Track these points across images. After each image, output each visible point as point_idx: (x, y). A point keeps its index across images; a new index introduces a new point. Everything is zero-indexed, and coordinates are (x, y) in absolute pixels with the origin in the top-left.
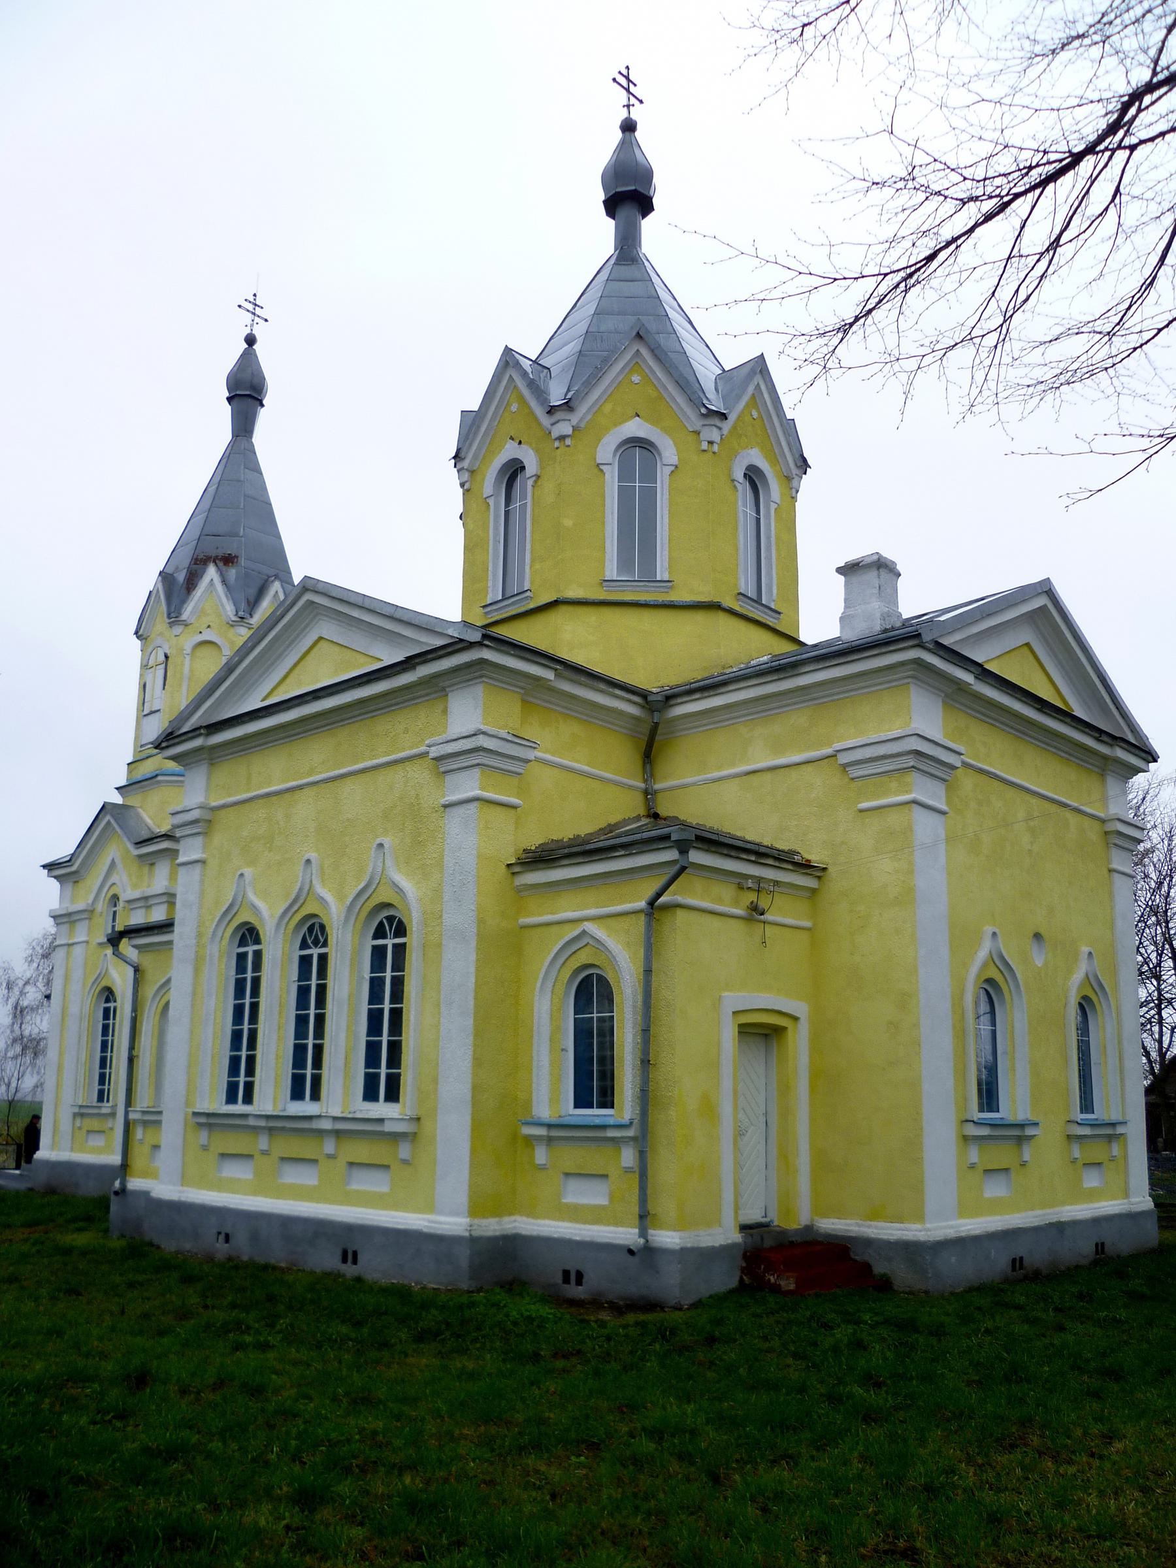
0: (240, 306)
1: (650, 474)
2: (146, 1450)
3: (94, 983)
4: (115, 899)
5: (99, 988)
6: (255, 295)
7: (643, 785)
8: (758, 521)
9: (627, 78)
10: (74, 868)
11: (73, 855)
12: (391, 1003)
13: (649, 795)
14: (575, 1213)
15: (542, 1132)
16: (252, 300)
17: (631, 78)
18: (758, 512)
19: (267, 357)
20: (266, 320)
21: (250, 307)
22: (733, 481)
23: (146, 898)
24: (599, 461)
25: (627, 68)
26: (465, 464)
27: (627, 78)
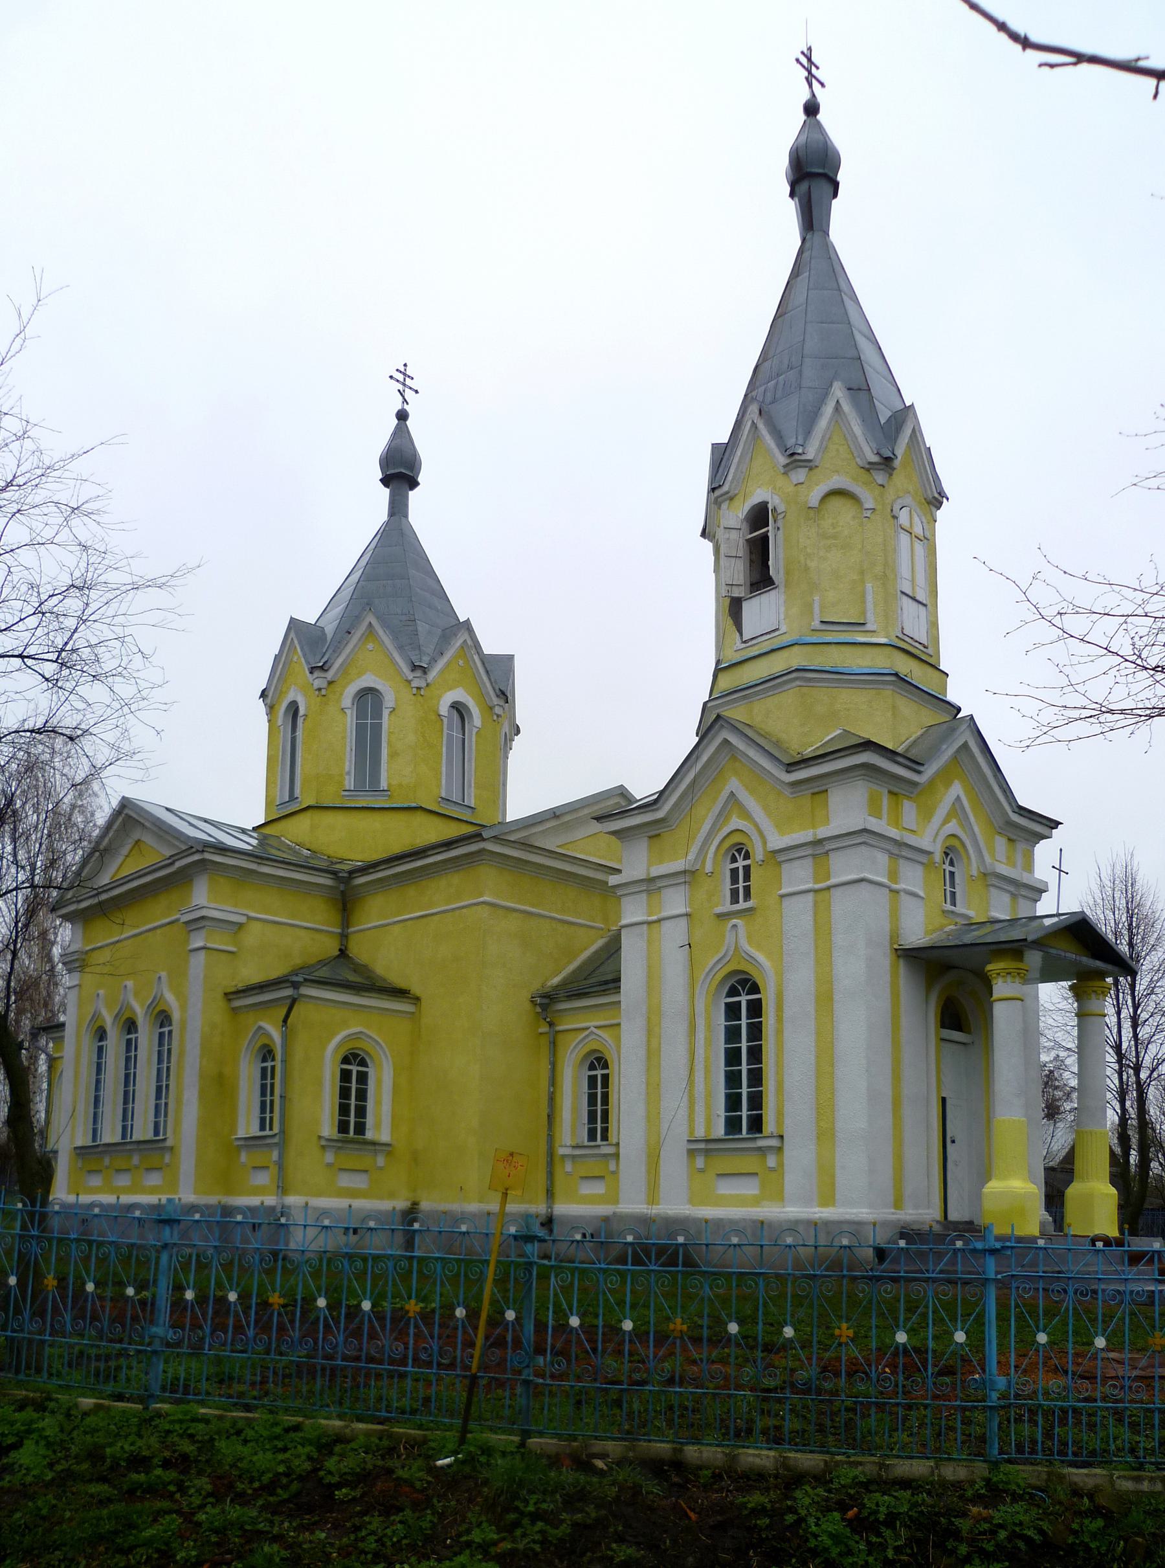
0: (391, 377)
1: (378, 714)
2: (856, 1483)
3: (91, 1021)
4: (740, 850)
5: (96, 1028)
6: (405, 365)
7: (339, 931)
8: (464, 740)
9: (809, 59)
10: (660, 814)
11: (662, 793)
12: (748, 1019)
13: (344, 937)
14: (586, 1200)
15: (702, 1146)
16: (403, 370)
17: (813, 59)
18: (464, 735)
19: (418, 430)
20: (417, 392)
21: (400, 377)
22: (439, 715)
23: (819, 842)
24: (343, 706)
25: (405, 365)
26: (268, 701)
27: (809, 59)
